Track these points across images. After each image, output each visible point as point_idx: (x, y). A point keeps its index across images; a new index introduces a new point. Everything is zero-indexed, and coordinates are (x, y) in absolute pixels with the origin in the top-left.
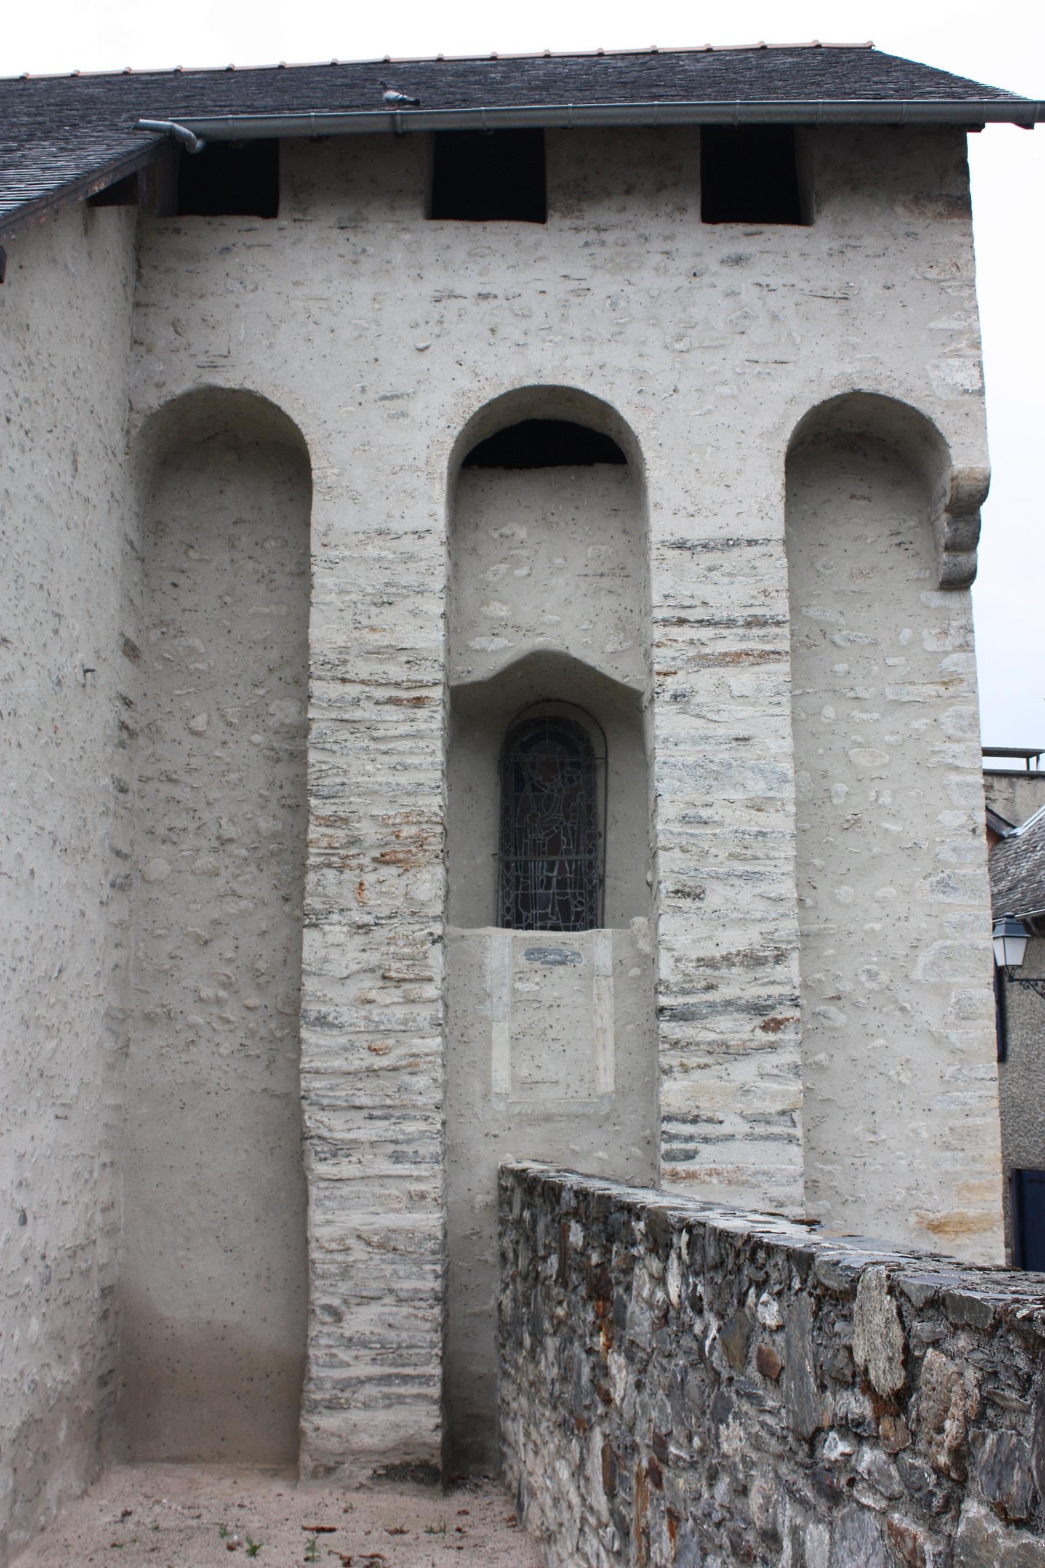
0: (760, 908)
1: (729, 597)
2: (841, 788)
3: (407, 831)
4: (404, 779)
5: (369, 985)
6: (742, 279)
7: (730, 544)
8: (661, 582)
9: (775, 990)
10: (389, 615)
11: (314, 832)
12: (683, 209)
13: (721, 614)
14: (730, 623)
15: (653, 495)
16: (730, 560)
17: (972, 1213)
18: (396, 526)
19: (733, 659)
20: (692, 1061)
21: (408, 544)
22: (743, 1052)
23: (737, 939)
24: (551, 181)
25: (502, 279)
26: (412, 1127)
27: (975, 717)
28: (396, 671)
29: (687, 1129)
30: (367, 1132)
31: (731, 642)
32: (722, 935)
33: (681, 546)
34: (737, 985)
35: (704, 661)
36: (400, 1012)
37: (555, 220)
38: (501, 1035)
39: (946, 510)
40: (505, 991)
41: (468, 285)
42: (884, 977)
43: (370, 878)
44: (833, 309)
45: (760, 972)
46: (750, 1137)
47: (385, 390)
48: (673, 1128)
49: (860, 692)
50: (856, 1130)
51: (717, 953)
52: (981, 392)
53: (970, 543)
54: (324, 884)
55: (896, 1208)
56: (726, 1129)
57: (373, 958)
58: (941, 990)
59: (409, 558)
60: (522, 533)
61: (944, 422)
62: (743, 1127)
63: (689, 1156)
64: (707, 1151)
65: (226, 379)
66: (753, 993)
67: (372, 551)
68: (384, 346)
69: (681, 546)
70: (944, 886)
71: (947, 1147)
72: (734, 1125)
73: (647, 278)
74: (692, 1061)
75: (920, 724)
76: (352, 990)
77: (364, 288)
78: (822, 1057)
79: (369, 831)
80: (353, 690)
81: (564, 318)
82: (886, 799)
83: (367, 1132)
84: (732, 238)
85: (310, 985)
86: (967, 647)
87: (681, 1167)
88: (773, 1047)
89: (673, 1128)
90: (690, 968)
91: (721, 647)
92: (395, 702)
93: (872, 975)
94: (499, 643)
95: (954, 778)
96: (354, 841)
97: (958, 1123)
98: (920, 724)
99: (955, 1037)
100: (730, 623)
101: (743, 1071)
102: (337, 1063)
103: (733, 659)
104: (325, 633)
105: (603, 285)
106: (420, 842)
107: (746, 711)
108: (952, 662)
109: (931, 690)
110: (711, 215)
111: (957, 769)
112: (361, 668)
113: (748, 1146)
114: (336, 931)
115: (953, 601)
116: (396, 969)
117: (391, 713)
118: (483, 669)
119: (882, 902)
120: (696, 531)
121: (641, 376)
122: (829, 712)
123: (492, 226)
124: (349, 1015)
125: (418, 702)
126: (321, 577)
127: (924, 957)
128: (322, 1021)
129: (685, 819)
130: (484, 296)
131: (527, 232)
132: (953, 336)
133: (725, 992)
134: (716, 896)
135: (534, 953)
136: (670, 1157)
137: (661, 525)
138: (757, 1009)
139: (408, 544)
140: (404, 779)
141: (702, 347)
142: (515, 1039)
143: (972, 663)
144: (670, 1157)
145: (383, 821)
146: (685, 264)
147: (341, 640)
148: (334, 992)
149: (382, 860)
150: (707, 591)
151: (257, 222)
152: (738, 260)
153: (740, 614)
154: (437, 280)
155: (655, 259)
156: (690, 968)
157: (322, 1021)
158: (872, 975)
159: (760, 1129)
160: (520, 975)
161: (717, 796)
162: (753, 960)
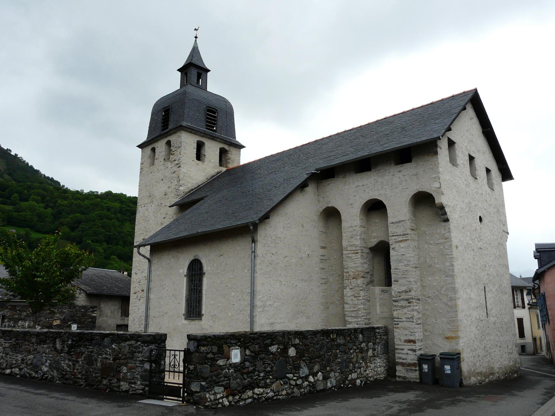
0: (407, 283)
1: (399, 231)
2: (428, 260)
3: (357, 273)
4: (355, 265)
5: (353, 298)
6: (400, 175)
7: (400, 222)
9: (409, 297)
10: (353, 240)
11: (345, 274)
13: (399, 234)
14: (400, 235)
15: (388, 215)
16: (400, 224)
17: (453, 336)
19: (401, 241)
20: (398, 309)
21: (354, 228)
22: (405, 307)
23: (403, 288)
25: (365, 182)
26: (359, 319)
27: (451, 245)
28: (354, 249)
29: (397, 320)
30: (353, 320)
31: (400, 239)
32: (401, 288)
33: (392, 223)
34: (404, 296)
35: (397, 242)
36: (357, 302)
37: (372, 170)
42: (437, 293)
43: (352, 281)
44: (415, 177)
46: (407, 321)
48: (395, 320)
49: (431, 242)
50: (27, 324)
53: (445, 213)
54: (346, 282)
55: (440, 334)
56: (403, 320)
57: (353, 293)
58: (447, 295)
59: (354, 230)
60: (377, 221)
62: (406, 320)
63: (398, 324)
65: (330, 205)
66: (406, 297)
67: (350, 230)
68: (349, 196)
69: (392, 223)
70: (447, 276)
71: (449, 323)
72: (404, 319)
73: (387, 178)
74: (398, 309)
75: (442, 247)
76: (350, 298)
77: (347, 187)
78: (427, 307)
79: (351, 273)
80: (348, 252)
81: (374, 187)
82: (436, 261)
83: (353, 320)
84: (399, 168)
85: (345, 298)
86: (449, 232)
87: (397, 326)
88: (409, 306)
89: (395, 320)
90: (396, 293)
91: (399, 239)
93: (434, 293)
95: (448, 256)
96: (350, 275)
97: (451, 319)
98: (442, 247)
99: (449, 303)
100: (400, 235)
101: (405, 310)
103: (401, 241)
104: (345, 243)
105: (380, 180)
106: (358, 275)
107: (403, 250)
109: (443, 240)
111: (448, 255)
112: (349, 248)
114: (348, 290)
115: (446, 224)
116: (356, 295)
117: (354, 255)
119: (436, 280)
120: (394, 221)
121: (386, 195)
122: (426, 246)
124: (350, 302)
125: (357, 253)
126: (344, 235)
127: (443, 289)
128: (347, 303)
129: (395, 269)
131: (368, 173)
132: (435, 178)
133: (402, 297)
134: (400, 282)
136: (395, 324)
137: (390, 220)
138: (407, 300)
140: (355, 265)
141: (395, 187)
143: (450, 235)
144: (395, 324)
145: (353, 272)
146: (392, 174)
147: (346, 244)
149: (353, 278)
150: (397, 230)
151: (332, 179)
152: (400, 171)
153: (402, 234)
154: (357, 184)
155: (388, 174)
156: (396, 293)
157: (347, 303)
158: (434, 293)
159: (408, 320)
161: (400, 265)
162: (406, 292)
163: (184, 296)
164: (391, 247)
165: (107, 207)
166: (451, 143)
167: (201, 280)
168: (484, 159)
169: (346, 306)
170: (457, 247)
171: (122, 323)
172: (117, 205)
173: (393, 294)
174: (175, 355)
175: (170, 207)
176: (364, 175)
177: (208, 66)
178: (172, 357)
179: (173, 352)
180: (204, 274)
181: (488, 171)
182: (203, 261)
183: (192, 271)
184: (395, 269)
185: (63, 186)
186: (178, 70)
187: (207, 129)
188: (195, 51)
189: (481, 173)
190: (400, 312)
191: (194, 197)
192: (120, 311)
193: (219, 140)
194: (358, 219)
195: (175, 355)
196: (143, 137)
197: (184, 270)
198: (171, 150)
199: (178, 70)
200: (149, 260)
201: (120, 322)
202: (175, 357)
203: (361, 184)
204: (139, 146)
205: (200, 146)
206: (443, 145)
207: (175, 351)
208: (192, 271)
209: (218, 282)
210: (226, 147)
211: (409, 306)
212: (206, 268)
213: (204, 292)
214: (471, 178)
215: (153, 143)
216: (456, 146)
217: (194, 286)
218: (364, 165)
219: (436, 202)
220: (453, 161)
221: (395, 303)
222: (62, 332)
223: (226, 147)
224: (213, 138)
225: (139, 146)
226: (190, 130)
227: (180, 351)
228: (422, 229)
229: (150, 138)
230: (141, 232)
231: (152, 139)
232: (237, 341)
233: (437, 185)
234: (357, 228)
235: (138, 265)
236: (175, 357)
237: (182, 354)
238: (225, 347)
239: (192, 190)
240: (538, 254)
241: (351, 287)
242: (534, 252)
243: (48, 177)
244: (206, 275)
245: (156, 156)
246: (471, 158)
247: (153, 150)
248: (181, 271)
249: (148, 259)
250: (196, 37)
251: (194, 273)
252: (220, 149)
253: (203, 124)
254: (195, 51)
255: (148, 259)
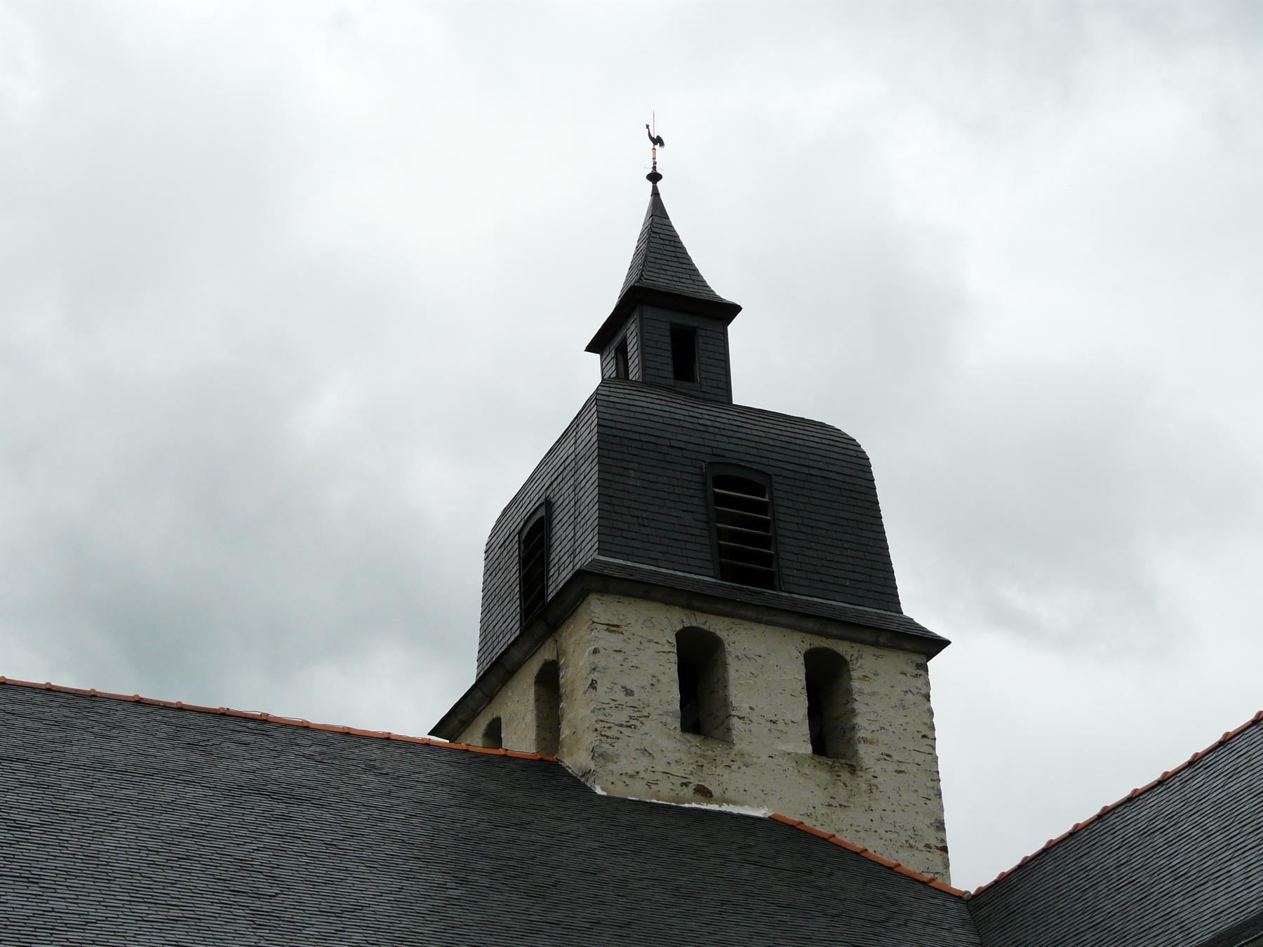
177: (722, 286)
188: (659, 238)
205: (699, 668)
250: (654, 177)
254: (659, 238)
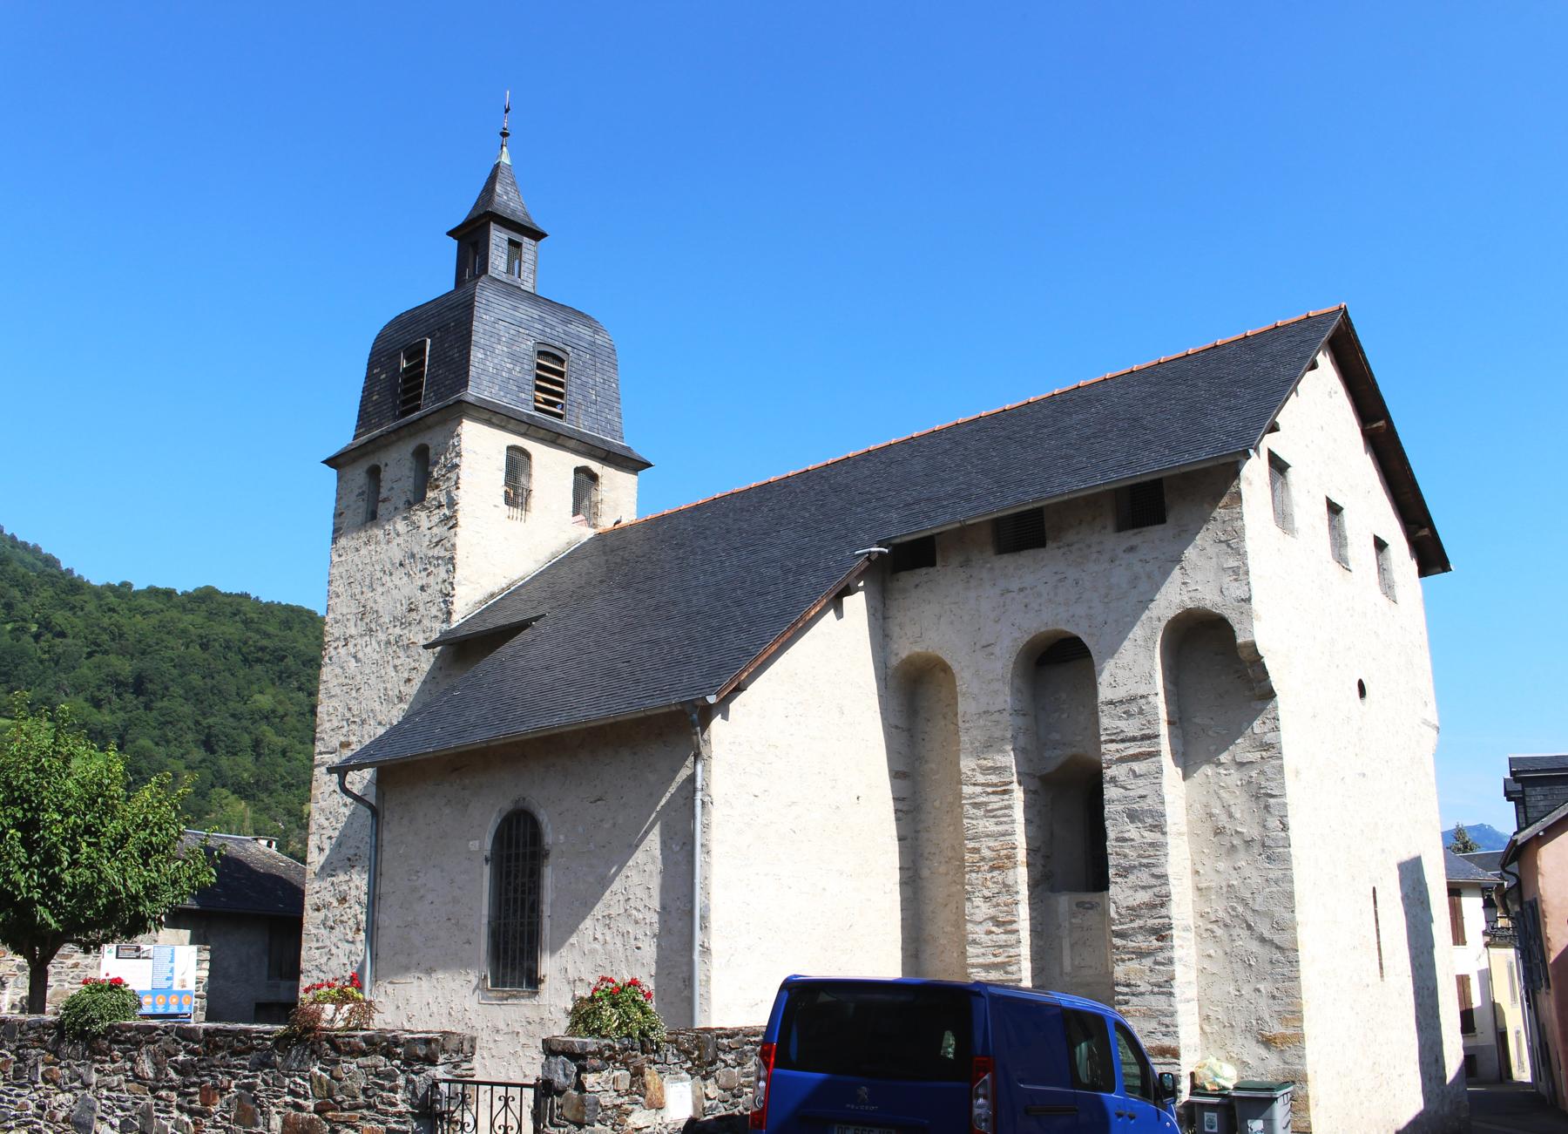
3: (1003, 853)
5: (989, 926)
7: (1132, 699)
8: (1105, 721)
12: (1104, 528)
14: (1134, 739)
18: (992, 708)
19: (1136, 758)
22: (1149, 954)
24: (1047, 525)
27: (1281, 766)
28: (994, 779)
29: (1125, 990)
31: (1134, 749)
33: (1111, 703)
35: (1122, 760)
36: (1004, 937)
38: (1066, 944)
39: (533, 982)
40: (1067, 924)
41: (1015, 586)
45: (1154, 912)
47: (984, 643)
51: (1135, 904)
52: (1249, 600)
56: (1142, 989)
57: (992, 912)
61: (1232, 617)
63: (1127, 1003)
64: (1134, 1000)
74: (1126, 957)
84: (1131, 538)
85: (969, 927)
86: (1276, 729)
91: (1131, 752)
92: (994, 793)
94: (1058, 752)
95: (1272, 801)
100: (1134, 739)
102: (981, 960)
103: (1136, 758)
108: (1269, 738)
109: (1258, 755)
110: (1121, 527)
112: (981, 779)
113: (1152, 997)
117: (993, 798)
118: (1051, 767)
123: (1025, 553)
124: (985, 938)
128: (974, 942)
129: (1118, 840)
130: (1021, 590)
131: (1040, 553)
135: (1080, 904)
139: (996, 717)
142: (1072, 946)
148: (977, 928)
149: (992, 869)
150: (1122, 724)
152: (1131, 549)
153: (1138, 734)
155: (1094, 556)
157: (974, 942)
160: (1074, 915)
163: (485, 920)
164: (1108, 773)
165: (201, 637)
166: (1278, 466)
167: (535, 876)
168: (1373, 511)
169: (971, 950)
170: (1297, 773)
171: (272, 998)
172: (230, 630)
173: (1113, 914)
174: (506, 1099)
175: (426, 647)
176: (1026, 557)
178: (498, 1105)
179: (500, 1091)
180: (547, 855)
181: (1380, 545)
182: (544, 817)
183: (509, 846)
184: (1118, 840)
185: (70, 571)
186: (449, 234)
187: (537, 409)
189: (1361, 551)
190: (1134, 965)
191: (501, 620)
192: (266, 960)
193: (572, 443)
194: (1007, 690)
195: (506, 1099)
196: (343, 435)
197: (484, 843)
198: (429, 474)
199: (449, 234)
200: (375, 812)
201: (266, 996)
202: (506, 1104)
203: (1015, 586)
204: (330, 462)
205: (517, 463)
206: (1255, 471)
207: (507, 1085)
208: (509, 846)
209: (591, 879)
210: (595, 466)
211: (1161, 949)
212: (551, 836)
213: (546, 910)
214: (1334, 567)
215: (373, 452)
216: (1292, 474)
217: (516, 891)
218: (1023, 533)
219: (1240, 640)
220: (1283, 517)
221: (1118, 942)
222: (156, 1028)
223: (595, 466)
224: (555, 439)
225: (330, 462)
226: (486, 416)
227: (522, 1086)
228: (1197, 720)
229: (364, 439)
230: (336, 724)
231: (370, 441)
232: (683, 1057)
233: (1237, 591)
234: (1006, 717)
235: (326, 824)
236: (506, 1104)
237: (529, 1094)
238: (651, 1075)
239: (492, 596)
240: (1519, 787)
241: (987, 893)
242: (1506, 781)
243: (25, 545)
244: (551, 859)
245: (384, 493)
246: (1334, 509)
247: (374, 473)
248: (474, 845)
249: (370, 806)
251: (513, 851)
252: (577, 470)
253: (529, 394)
255: (370, 806)
